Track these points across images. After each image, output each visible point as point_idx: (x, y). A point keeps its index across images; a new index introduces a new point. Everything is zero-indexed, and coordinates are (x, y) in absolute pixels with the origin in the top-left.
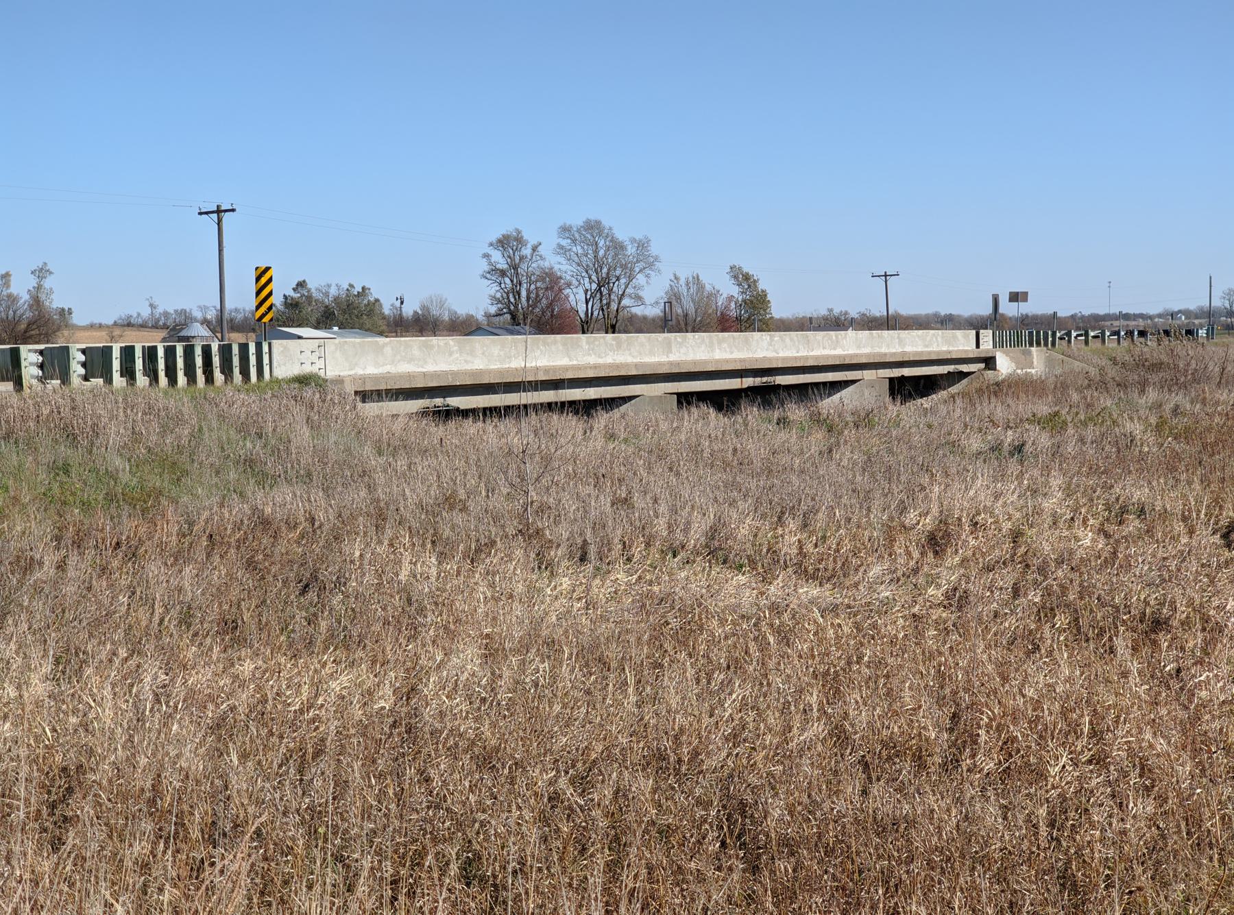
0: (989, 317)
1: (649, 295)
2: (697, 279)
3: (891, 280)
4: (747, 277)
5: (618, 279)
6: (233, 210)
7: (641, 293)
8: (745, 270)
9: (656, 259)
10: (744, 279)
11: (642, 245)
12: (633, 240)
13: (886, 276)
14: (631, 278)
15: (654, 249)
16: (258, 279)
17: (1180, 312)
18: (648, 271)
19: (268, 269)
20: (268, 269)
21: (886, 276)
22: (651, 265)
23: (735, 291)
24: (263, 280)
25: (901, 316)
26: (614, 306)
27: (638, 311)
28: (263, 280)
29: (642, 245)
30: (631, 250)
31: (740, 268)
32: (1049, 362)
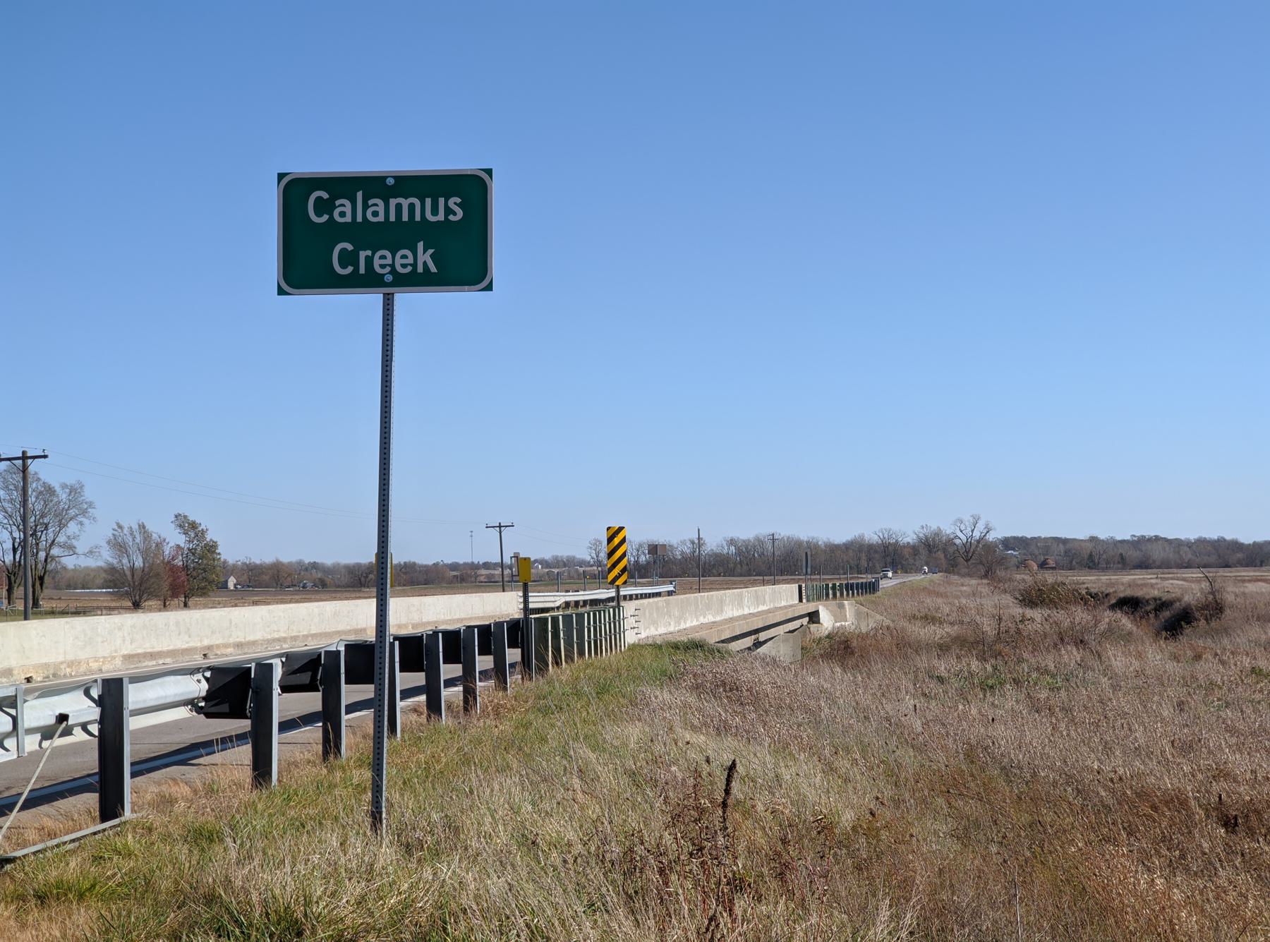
0: (369, 569)
1: (85, 547)
2: (142, 527)
3: (505, 532)
4: (193, 526)
5: (46, 529)
6: (45, 457)
7: (75, 542)
8: (191, 518)
9: (91, 505)
10: (188, 526)
11: (75, 491)
12: (64, 486)
13: (500, 527)
14: (62, 526)
15: (88, 494)
16: (610, 540)
17: (536, 561)
18: (80, 518)
19: (621, 529)
20: (621, 529)
21: (500, 527)
22: (84, 512)
23: (181, 540)
24: (616, 541)
25: (282, 564)
26: (42, 555)
27: (69, 562)
28: (616, 541)
29: (75, 491)
30: (63, 496)
31: (185, 517)
32: (858, 615)
